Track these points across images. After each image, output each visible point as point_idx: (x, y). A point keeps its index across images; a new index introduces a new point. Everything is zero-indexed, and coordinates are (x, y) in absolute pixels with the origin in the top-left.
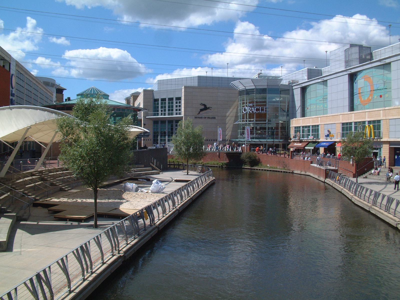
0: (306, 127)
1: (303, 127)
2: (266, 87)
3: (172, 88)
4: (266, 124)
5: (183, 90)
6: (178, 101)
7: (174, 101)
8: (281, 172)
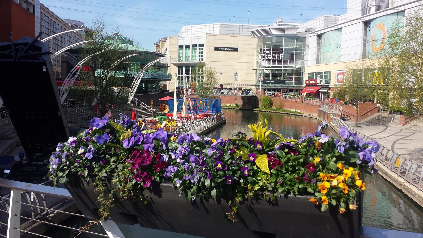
0: (319, 73)
1: (316, 73)
3: (196, 35)
4: (281, 70)
6: (201, 48)
7: (198, 48)
8: (234, 109)
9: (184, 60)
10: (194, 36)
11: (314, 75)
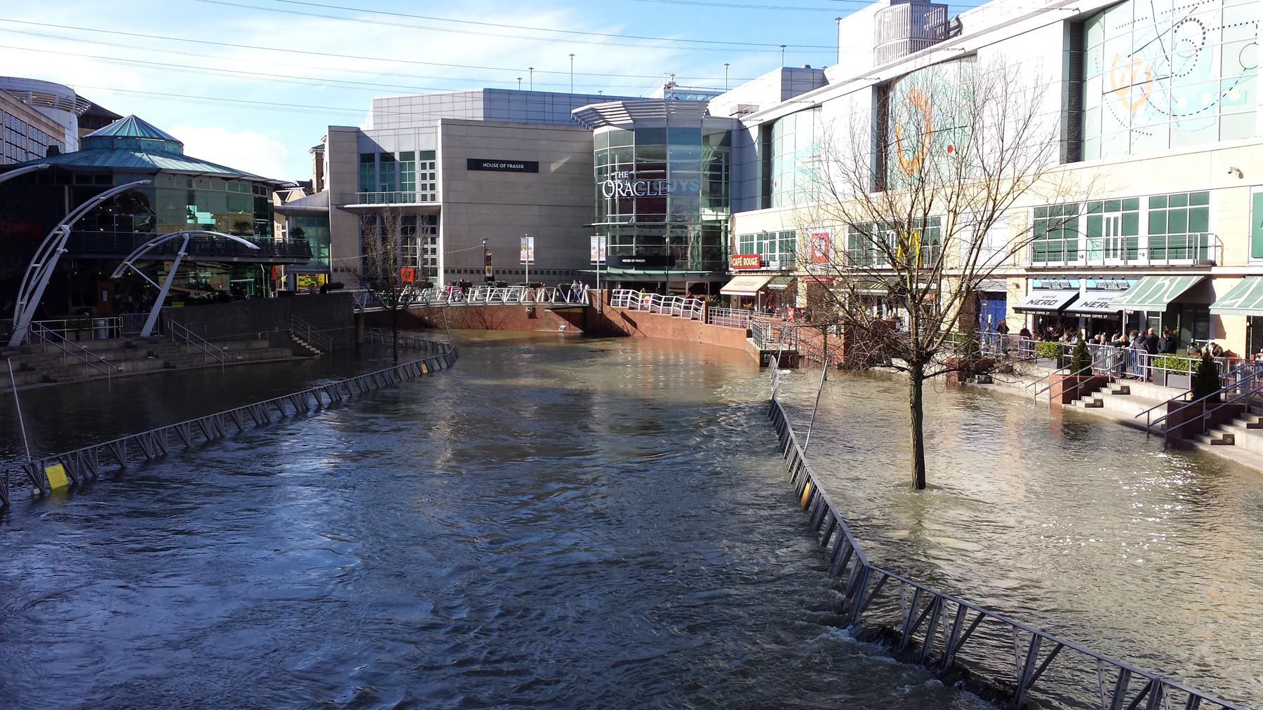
0: (1112, 205)
1: (1095, 207)
2: (663, 125)
5: (440, 130)
6: (428, 162)
9: (418, 197)
10: (408, 125)
11: (755, 242)
